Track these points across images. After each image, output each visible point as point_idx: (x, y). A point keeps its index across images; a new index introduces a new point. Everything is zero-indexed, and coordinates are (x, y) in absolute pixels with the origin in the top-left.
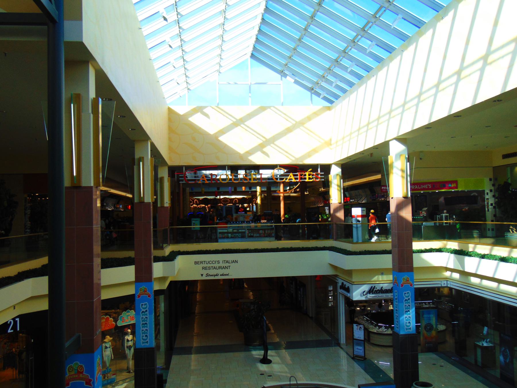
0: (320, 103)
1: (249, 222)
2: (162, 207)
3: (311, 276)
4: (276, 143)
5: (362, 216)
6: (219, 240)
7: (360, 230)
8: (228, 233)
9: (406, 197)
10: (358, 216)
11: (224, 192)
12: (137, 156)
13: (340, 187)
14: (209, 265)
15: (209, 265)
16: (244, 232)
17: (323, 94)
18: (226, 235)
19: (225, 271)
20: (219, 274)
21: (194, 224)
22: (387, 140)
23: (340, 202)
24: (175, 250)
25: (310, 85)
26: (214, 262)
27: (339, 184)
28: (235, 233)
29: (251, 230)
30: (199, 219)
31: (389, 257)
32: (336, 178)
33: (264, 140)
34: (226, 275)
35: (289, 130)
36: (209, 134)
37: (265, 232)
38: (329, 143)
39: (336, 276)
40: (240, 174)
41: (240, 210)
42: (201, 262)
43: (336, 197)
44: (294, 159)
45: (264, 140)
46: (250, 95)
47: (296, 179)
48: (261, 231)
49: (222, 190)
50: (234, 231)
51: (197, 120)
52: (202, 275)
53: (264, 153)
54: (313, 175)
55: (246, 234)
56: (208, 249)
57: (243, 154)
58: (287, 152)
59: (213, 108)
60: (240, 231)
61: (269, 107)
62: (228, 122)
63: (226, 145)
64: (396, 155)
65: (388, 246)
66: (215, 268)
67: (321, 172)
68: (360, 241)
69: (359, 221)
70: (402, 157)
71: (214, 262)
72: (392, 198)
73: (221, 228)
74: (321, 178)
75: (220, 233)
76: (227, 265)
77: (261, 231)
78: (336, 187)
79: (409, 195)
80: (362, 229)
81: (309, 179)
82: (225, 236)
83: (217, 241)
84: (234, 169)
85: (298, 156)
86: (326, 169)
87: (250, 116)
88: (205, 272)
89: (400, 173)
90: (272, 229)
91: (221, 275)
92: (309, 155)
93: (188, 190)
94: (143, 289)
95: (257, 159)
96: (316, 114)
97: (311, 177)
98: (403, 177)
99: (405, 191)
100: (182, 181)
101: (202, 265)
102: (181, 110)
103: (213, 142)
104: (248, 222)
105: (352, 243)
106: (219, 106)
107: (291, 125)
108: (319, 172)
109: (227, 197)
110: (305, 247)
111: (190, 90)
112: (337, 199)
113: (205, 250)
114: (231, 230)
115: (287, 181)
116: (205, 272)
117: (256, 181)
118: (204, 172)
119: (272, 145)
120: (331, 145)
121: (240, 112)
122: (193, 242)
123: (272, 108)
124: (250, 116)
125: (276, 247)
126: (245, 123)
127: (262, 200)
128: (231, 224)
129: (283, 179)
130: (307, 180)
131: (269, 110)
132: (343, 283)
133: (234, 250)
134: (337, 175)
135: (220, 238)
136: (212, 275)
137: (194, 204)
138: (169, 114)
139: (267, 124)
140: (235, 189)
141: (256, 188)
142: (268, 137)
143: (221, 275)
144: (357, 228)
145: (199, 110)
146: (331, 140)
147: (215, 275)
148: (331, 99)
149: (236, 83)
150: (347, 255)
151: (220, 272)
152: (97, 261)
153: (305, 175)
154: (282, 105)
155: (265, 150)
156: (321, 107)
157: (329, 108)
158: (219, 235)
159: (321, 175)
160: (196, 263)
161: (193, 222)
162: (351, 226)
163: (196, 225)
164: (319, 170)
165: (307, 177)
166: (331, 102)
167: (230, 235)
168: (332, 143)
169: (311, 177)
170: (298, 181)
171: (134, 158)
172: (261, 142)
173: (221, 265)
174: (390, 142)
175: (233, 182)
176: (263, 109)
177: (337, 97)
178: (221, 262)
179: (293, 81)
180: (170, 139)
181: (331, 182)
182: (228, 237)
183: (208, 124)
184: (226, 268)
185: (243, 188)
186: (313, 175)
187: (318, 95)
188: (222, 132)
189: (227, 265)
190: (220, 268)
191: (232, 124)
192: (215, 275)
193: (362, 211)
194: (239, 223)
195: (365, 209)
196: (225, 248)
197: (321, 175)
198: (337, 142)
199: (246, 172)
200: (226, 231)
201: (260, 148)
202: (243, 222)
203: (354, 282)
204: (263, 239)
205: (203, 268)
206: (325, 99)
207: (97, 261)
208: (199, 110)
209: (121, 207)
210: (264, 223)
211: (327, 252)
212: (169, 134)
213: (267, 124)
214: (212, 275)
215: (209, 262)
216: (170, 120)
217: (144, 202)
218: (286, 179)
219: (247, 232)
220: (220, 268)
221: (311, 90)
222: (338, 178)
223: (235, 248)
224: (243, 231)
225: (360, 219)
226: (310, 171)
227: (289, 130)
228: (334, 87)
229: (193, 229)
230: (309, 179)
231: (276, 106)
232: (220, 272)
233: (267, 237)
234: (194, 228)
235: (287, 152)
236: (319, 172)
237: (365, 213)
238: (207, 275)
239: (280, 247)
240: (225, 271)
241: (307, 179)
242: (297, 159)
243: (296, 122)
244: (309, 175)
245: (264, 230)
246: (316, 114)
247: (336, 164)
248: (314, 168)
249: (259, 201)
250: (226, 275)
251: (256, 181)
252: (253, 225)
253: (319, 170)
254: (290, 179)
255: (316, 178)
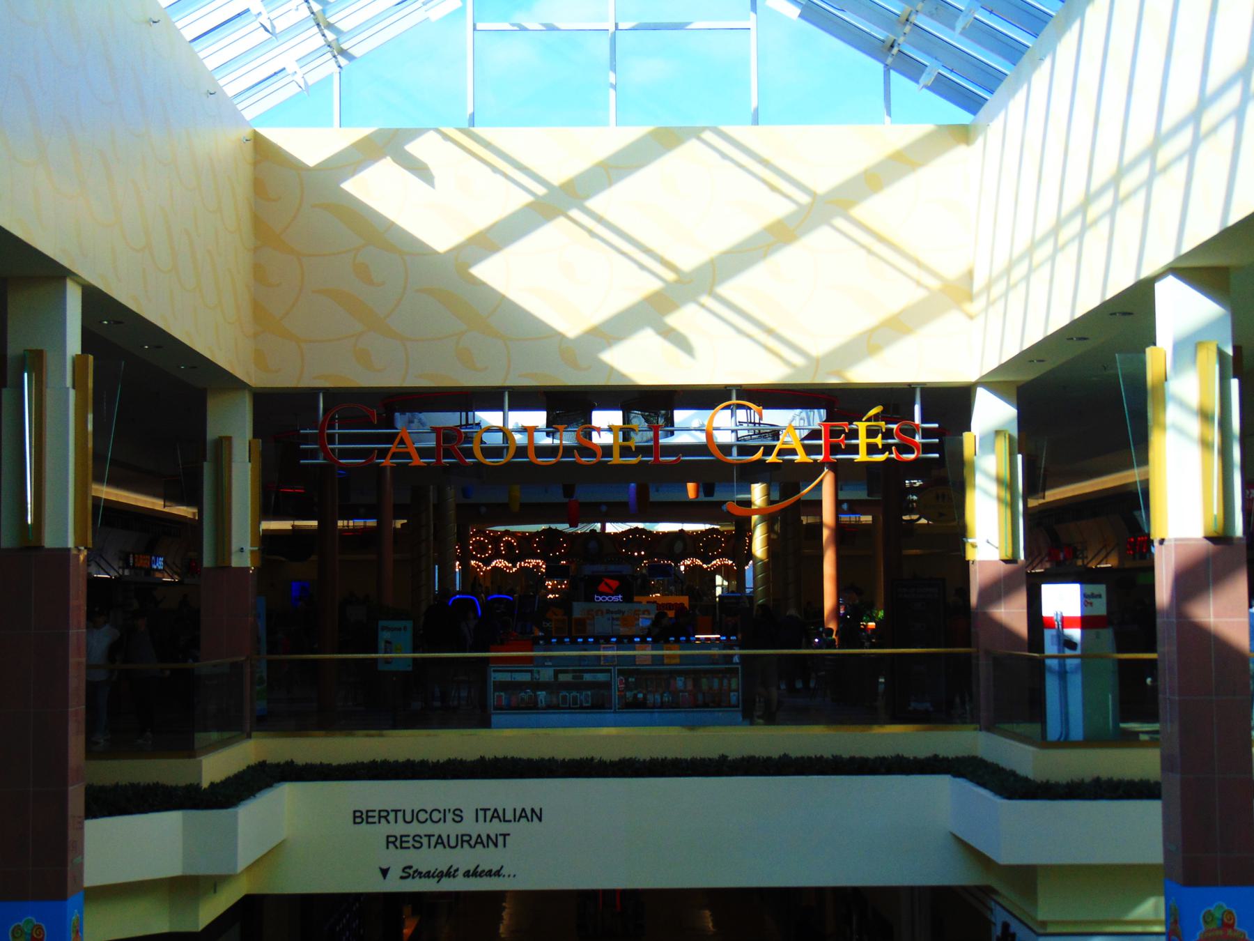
0: (924, 110)
1: (630, 639)
2: (223, 567)
3: (912, 889)
4: (724, 290)
5: (1086, 622)
6: (495, 719)
7: (1075, 681)
8: (537, 686)
9: (1220, 539)
10: (1067, 622)
11: (610, 505)
12: (14, 348)
13: (1011, 486)
14: (415, 829)
15: (415, 829)
16: (607, 685)
17: (934, 68)
18: (525, 695)
19: (487, 858)
20: (451, 869)
21: (389, 647)
22: (1146, 273)
23: (1009, 555)
24: (271, 760)
25: (880, 34)
26: (422, 816)
27: (1006, 474)
28: (567, 686)
29: (635, 674)
30: (409, 624)
31: (1150, 813)
32: (993, 450)
33: (670, 276)
34: (489, 873)
35: (780, 235)
36: (437, 253)
37: (696, 683)
38: (960, 292)
39: (987, 891)
40: (599, 430)
41: (602, 588)
42: (383, 815)
43: (989, 532)
44: (799, 361)
45: (670, 276)
46: (612, 78)
47: (809, 450)
48: (680, 682)
49: (584, 494)
50: (563, 678)
51: (379, 190)
52: (384, 872)
53: (671, 335)
54: (888, 434)
55: (615, 694)
56: (417, 757)
57: (579, 339)
58: (770, 332)
59: (446, 137)
60: (588, 677)
61: (695, 133)
62: (507, 200)
63: (503, 297)
64: (1178, 346)
65: (1142, 762)
66: (439, 841)
67: (923, 421)
68: (1077, 733)
69: (1070, 644)
70: (1202, 355)
71: (436, 816)
72: (1162, 541)
73: (506, 663)
74: (927, 448)
75: (502, 686)
76: (496, 827)
77: (680, 682)
78: (993, 488)
79: (1239, 530)
80: (1084, 678)
81: (872, 449)
82: (525, 703)
83: (486, 724)
84: (569, 405)
85: (818, 348)
86: (951, 405)
87: (611, 171)
88: (397, 859)
89: (1194, 426)
90: (733, 672)
91: (467, 874)
92: (869, 343)
93: (452, 496)
94: (1218, 914)
95: (643, 362)
96: (904, 162)
97: (879, 441)
98: (1205, 444)
99: (1216, 509)
100: (313, 454)
101: (384, 829)
102: (309, 145)
103: (443, 284)
104: (625, 641)
105: (1043, 742)
106: (475, 130)
107: (789, 208)
108: (917, 420)
109: (641, 525)
110: (846, 755)
111: (350, 58)
112: (995, 540)
113: (402, 759)
114: (546, 674)
115: (772, 459)
116: (397, 859)
117: (633, 460)
118: (491, 418)
119: (706, 300)
120: (971, 297)
121: (562, 152)
122: (445, 724)
123: (707, 136)
124: (611, 171)
125: (714, 755)
126: (591, 204)
127: (770, 543)
128: (574, 644)
129: (754, 450)
130: (862, 457)
131: (692, 145)
132: (1006, 926)
133: (530, 761)
134: (997, 433)
135: (499, 708)
136: (428, 875)
137: (497, 555)
138: (256, 164)
139: (688, 205)
140: (643, 492)
141: (749, 492)
142: (688, 261)
143: (467, 874)
144: (1063, 674)
145: (387, 145)
146: (970, 275)
147: (441, 875)
148: (971, 90)
149: (550, 28)
150: (1010, 798)
151: (465, 858)
152: (76, 798)
153: (854, 434)
154: (756, 121)
155: (672, 320)
156: (928, 127)
157: (964, 134)
158: (493, 697)
159: (926, 433)
160: (360, 817)
161: (385, 635)
162: (1039, 668)
163: (397, 652)
164: (917, 408)
165: (862, 441)
166: (972, 103)
167: (542, 695)
168: (978, 284)
169: (879, 441)
170: (820, 458)
171: (5, 356)
172: (656, 285)
173: (469, 826)
174: (1159, 286)
175: (530, 465)
176: (665, 139)
177: (992, 80)
178: (469, 815)
179: (797, 11)
180: (259, 273)
181: (972, 465)
182: (532, 706)
183: (425, 207)
184: (491, 841)
185: (691, 487)
186: (888, 434)
187: (913, 70)
188: (488, 242)
189: (496, 827)
190: (464, 840)
191: (529, 206)
192: (441, 875)
193: (1086, 599)
194: (585, 646)
195: (1101, 589)
196: (489, 755)
197: (926, 433)
198: (988, 287)
199: (626, 420)
200: (526, 677)
201: (652, 312)
202: (602, 640)
203: (1044, 924)
204: (544, 717)
205: (391, 841)
206: (943, 87)
207: (76, 798)
208: (387, 145)
209: (159, 564)
210: (706, 644)
211: (943, 784)
212: (256, 250)
213: (688, 205)
214: (428, 875)
215: (415, 815)
216: (259, 187)
217: (40, 548)
218: (768, 450)
219: (617, 683)
220: (464, 840)
221: (884, 51)
222: (1002, 446)
223: (535, 756)
224: (601, 677)
225: (1075, 633)
226: (876, 418)
227: (780, 235)
228: (964, 33)
229: (382, 667)
230: (872, 449)
231: (724, 128)
232: (465, 858)
233: (706, 705)
234: (387, 661)
235: (770, 332)
236: (917, 420)
237: (1100, 608)
238: (408, 872)
239: (734, 753)
240: (487, 858)
241: (863, 449)
242: (816, 362)
243: (812, 194)
244: (871, 433)
245: (695, 675)
246: (904, 162)
247: (995, 383)
248: (894, 400)
249: (759, 547)
250: (489, 873)
251: (633, 460)
252: (645, 653)
253: (917, 408)
254: (782, 452)
255: (905, 448)
